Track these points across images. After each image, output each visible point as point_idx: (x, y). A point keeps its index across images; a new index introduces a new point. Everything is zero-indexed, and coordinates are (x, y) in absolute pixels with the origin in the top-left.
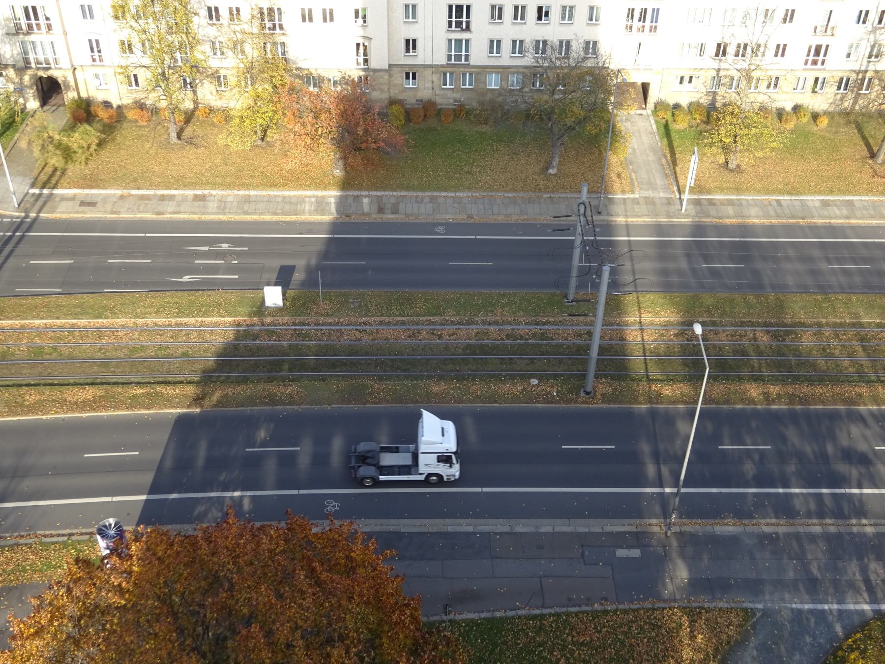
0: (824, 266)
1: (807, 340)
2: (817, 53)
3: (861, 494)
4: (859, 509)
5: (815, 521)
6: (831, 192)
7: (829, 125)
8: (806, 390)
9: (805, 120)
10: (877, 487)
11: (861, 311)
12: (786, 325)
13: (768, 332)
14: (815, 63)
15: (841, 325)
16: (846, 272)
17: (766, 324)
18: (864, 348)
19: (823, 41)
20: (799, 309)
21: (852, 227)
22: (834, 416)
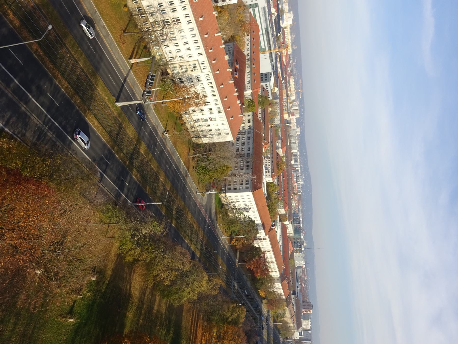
1: (62, 51)
3: (31, 99)
4: (27, 102)
6: (108, 26)
8: (48, 62)
10: (42, 107)
12: (62, 41)
15: (73, 57)
16: (89, 48)
17: (58, 35)
22: (47, 75)
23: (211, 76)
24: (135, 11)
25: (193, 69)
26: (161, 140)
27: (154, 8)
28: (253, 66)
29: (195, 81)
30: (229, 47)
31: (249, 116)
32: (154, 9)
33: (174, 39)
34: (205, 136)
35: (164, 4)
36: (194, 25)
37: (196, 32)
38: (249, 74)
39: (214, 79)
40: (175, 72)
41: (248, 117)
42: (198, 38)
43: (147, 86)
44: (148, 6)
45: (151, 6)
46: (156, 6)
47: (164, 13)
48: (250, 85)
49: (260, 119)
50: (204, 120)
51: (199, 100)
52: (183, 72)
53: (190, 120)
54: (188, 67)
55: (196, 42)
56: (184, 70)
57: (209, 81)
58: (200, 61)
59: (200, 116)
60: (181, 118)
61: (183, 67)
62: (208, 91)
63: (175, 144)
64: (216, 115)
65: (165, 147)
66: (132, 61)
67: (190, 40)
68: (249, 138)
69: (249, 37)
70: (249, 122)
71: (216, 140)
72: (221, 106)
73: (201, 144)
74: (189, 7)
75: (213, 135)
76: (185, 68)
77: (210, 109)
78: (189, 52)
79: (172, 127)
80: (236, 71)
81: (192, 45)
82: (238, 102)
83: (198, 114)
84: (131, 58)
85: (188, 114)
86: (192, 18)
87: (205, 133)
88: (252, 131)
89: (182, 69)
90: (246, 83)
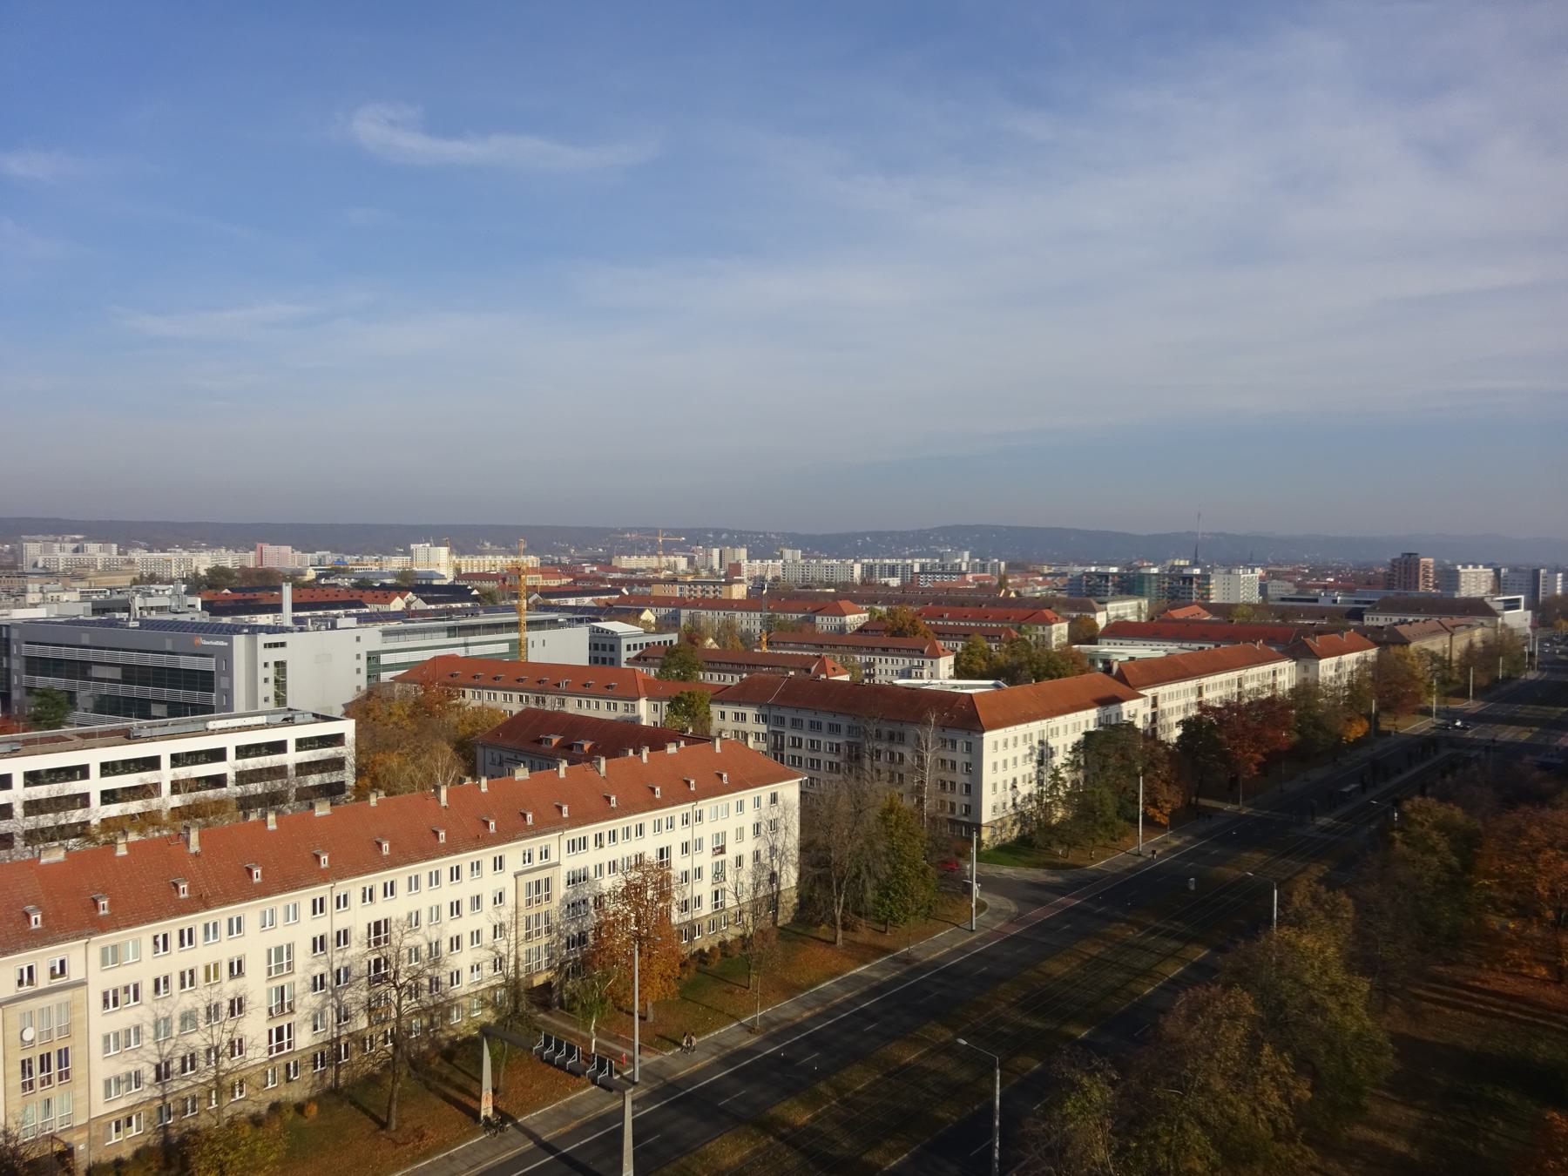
7: (320, 1111)
9: (290, 1116)
14: (280, 1048)
19: (284, 1022)
21: (700, 1071)
23: (575, 833)
24: (323, 1075)
26: (773, 1039)
27: (324, 1006)
28: (563, 686)
29: (586, 891)
30: (489, 760)
31: (723, 715)
32: (328, 1009)
33: (434, 948)
34: (773, 877)
35: (318, 971)
36: (400, 875)
37: (423, 869)
38: (585, 704)
40: (544, 958)
41: (725, 720)
42: (444, 864)
44: (315, 1028)
45: (315, 1018)
46: (320, 998)
47: (347, 974)
48: (620, 704)
49: (737, 678)
50: (719, 874)
51: (651, 884)
52: (549, 931)
55: (456, 873)
56: (543, 926)
57: (591, 841)
58: (520, 867)
59: (704, 888)
62: (623, 850)
63: (790, 990)
65: (797, 1028)
66: (487, 1109)
67: (448, 892)
68: (796, 724)
69: (468, 692)
70: (744, 715)
71: (791, 839)
72: (678, 811)
73: (799, 896)
74: (342, 886)
75: (773, 849)
77: (685, 848)
79: (731, 993)
80: (570, 747)
81: (464, 890)
82: (672, 749)
83: (696, 895)
85: (691, 929)
86: (377, 880)
87: (765, 877)
88: (775, 712)
89: (538, 933)
90: (611, 715)
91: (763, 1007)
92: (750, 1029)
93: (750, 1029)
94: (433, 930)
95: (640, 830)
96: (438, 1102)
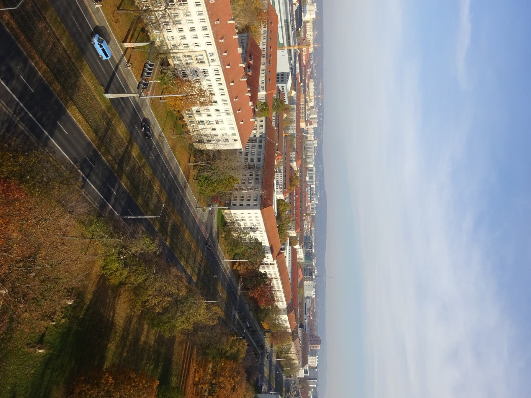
0: (71, 14)
1: (41, 26)
2: (201, 59)
5: (24, 125)
11: (65, 39)
12: (41, 14)
13: (33, 7)
15: (54, 34)
16: (74, 24)
17: (36, 5)
18: (52, 48)
20: (50, 14)
25: (200, 61)
26: (157, 143)
28: (269, 64)
29: (201, 76)
31: (262, 121)
34: (209, 141)
37: (206, 16)
38: (263, 72)
39: (224, 75)
40: (178, 63)
41: (260, 122)
42: (208, 24)
43: (143, 77)
48: (264, 85)
50: (209, 122)
51: (205, 99)
52: (187, 64)
53: (192, 121)
54: (193, 57)
55: (205, 28)
56: (188, 61)
57: (218, 77)
58: (208, 52)
59: (204, 117)
60: (182, 118)
61: (187, 58)
63: (173, 148)
64: (223, 117)
65: (162, 151)
66: (127, 45)
67: (198, 26)
68: (260, 147)
69: (265, 29)
70: (261, 129)
71: (222, 146)
72: (230, 107)
73: (204, 150)
75: (218, 141)
76: (189, 59)
77: (217, 110)
78: (196, 40)
81: (199, 32)
83: (202, 115)
84: (124, 41)
85: (191, 114)
87: (209, 138)
88: (263, 139)
89: (186, 60)
91: (167, 139)
92: (160, 136)
93: (160, 136)
94: (185, 21)
95: (223, 94)
96: (128, 28)
